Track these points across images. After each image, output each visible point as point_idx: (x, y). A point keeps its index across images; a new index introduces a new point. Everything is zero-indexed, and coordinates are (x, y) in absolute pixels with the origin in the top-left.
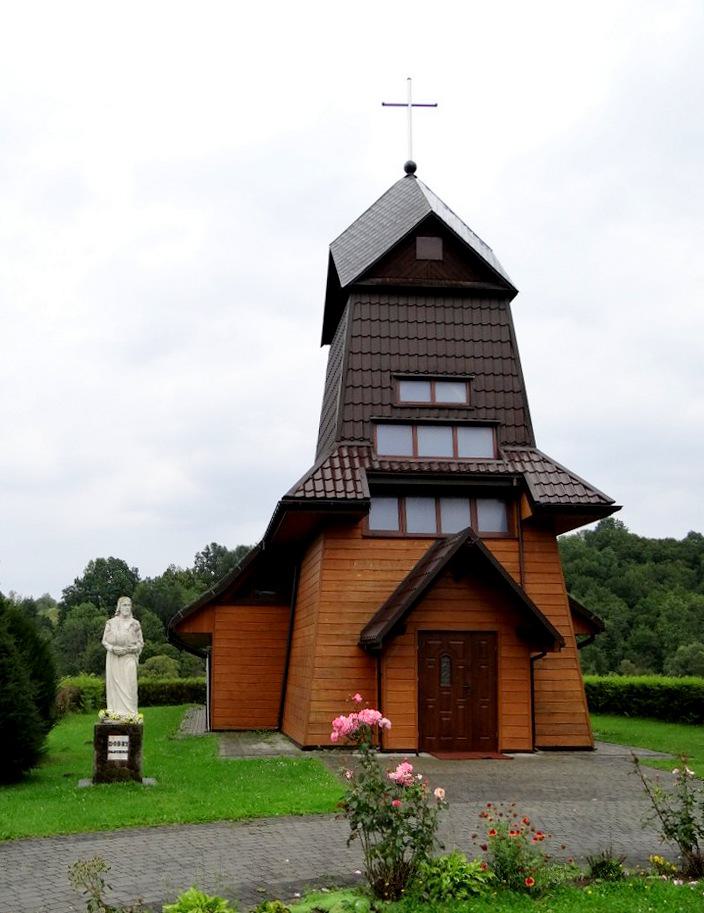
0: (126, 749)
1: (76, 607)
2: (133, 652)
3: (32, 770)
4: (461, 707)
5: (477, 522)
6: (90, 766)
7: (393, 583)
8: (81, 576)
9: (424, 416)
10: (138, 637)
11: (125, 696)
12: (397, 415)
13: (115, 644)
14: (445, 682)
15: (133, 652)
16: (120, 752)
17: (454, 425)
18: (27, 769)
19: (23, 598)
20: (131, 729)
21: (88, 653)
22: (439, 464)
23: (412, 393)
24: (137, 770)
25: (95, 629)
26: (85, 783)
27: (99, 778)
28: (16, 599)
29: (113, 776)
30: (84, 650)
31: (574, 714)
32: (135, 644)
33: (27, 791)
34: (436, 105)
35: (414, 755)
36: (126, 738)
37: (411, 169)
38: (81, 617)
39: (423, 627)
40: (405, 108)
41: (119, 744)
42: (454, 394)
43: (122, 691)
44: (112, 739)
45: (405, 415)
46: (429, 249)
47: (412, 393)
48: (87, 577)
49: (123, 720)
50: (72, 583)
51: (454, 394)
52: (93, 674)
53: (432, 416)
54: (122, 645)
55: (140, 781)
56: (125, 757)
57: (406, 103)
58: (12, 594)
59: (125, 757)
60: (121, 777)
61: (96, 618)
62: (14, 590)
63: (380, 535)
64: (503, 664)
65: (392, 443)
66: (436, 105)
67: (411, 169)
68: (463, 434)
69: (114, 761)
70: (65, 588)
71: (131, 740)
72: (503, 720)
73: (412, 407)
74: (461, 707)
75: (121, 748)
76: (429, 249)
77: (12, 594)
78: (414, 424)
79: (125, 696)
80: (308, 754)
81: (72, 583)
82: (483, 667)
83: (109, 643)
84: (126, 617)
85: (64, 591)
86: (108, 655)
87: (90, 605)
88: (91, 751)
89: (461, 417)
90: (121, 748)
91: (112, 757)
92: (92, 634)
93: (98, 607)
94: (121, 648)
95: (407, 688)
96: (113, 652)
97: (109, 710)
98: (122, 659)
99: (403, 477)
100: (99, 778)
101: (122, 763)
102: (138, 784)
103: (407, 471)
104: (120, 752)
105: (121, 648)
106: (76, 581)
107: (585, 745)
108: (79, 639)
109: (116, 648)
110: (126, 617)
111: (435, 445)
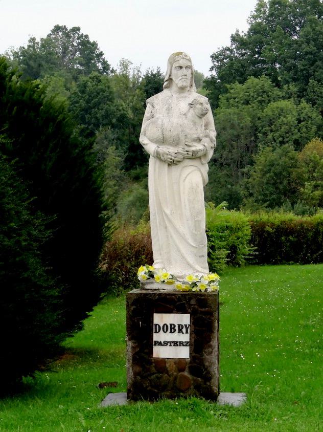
0: (185, 338)
1: (237, 85)
2: (195, 156)
3: (24, 378)
6: (124, 373)
8: (244, 29)
10: (207, 126)
11: (183, 238)
13: (162, 141)
15: (195, 156)
16: (175, 343)
18: (30, 372)
19: (143, 73)
20: (193, 302)
21: (258, 167)
24: (208, 377)
25: (271, 124)
26: (118, 399)
27: (137, 392)
28: (131, 74)
29: (164, 388)
30: (252, 163)
32: (199, 140)
33: (33, 408)
36: (185, 319)
38: (247, 102)
41: (172, 328)
43: (177, 231)
44: (159, 319)
48: (255, 30)
49: (179, 286)
50: (228, 43)
52: (224, 203)
54: (176, 142)
55: (212, 397)
56: (184, 353)
58: (125, 65)
59: (184, 353)
60: (176, 392)
61: (273, 105)
62: (127, 57)
69: (164, 361)
70: (215, 50)
71: (195, 321)
75: (176, 337)
77: (125, 65)
79: (183, 238)
80: (113, 380)
81: (228, 43)
83: (152, 141)
84: (182, 89)
85: (214, 57)
86: (152, 161)
87: (265, 82)
88: (125, 348)
90: (176, 337)
91: (160, 352)
92: (265, 134)
93: (278, 85)
94: (172, 150)
96: (158, 156)
97: (156, 267)
98: (173, 168)
100: (137, 392)
101: (179, 363)
102: (203, 404)
104: (175, 343)
105: (172, 150)
106: (235, 38)
108: (243, 142)
109: (163, 149)
110: (182, 89)
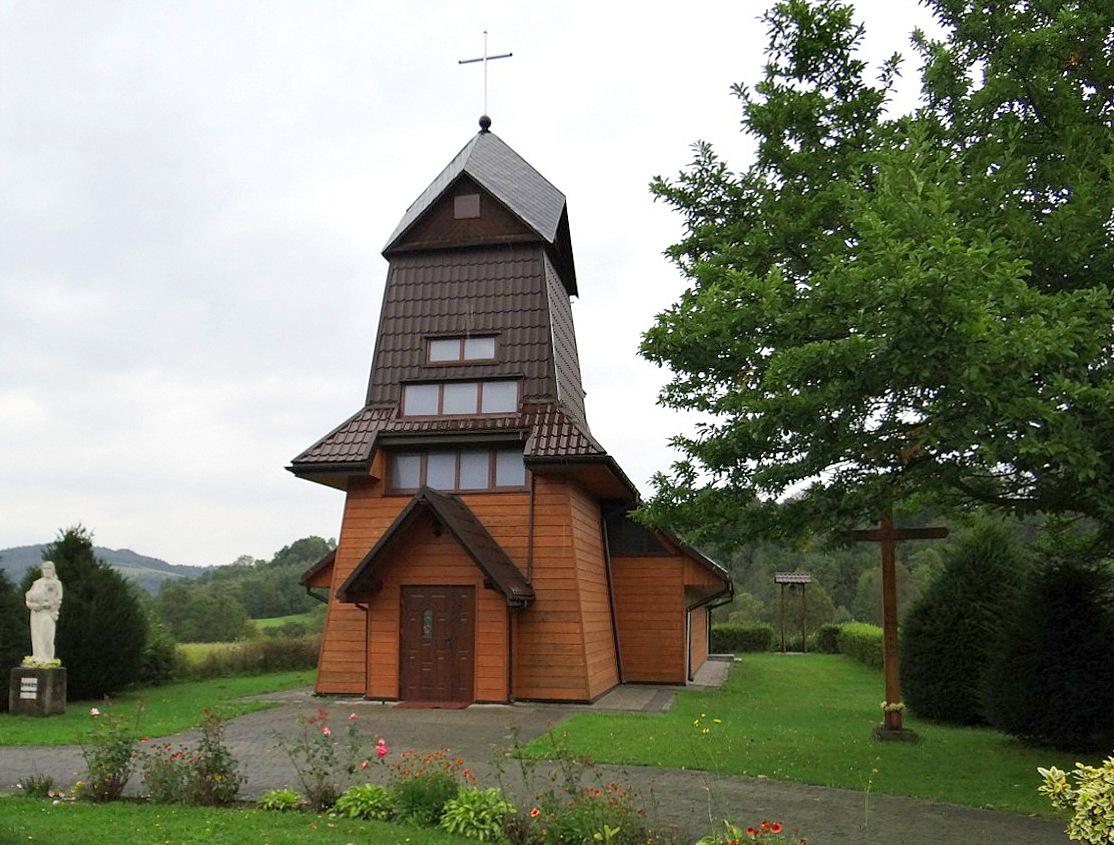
0: (35, 689)
4: (441, 658)
5: (426, 476)
7: (371, 540)
9: (451, 374)
12: (425, 375)
14: (428, 630)
17: (480, 380)
22: (466, 421)
23: (443, 352)
31: (572, 667)
34: (511, 55)
35: (381, 703)
36: (35, 681)
37: (485, 123)
39: (404, 583)
40: (489, 55)
41: (29, 685)
42: (483, 350)
44: (24, 680)
45: (433, 374)
46: (467, 207)
47: (443, 352)
51: (483, 350)
53: (459, 373)
54: (37, 601)
56: (34, 696)
57: (480, 57)
59: (34, 696)
63: (509, 490)
64: (480, 617)
65: (420, 403)
66: (511, 55)
67: (485, 123)
68: (489, 389)
72: (479, 672)
73: (439, 366)
74: (441, 658)
76: (467, 207)
78: (442, 382)
82: (463, 620)
89: (488, 372)
91: (24, 696)
94: (37, 605)
95: (389, 640)
99: (405, 437)
103: (490, 429)
107: (580, 698)
111: (461, 402)
